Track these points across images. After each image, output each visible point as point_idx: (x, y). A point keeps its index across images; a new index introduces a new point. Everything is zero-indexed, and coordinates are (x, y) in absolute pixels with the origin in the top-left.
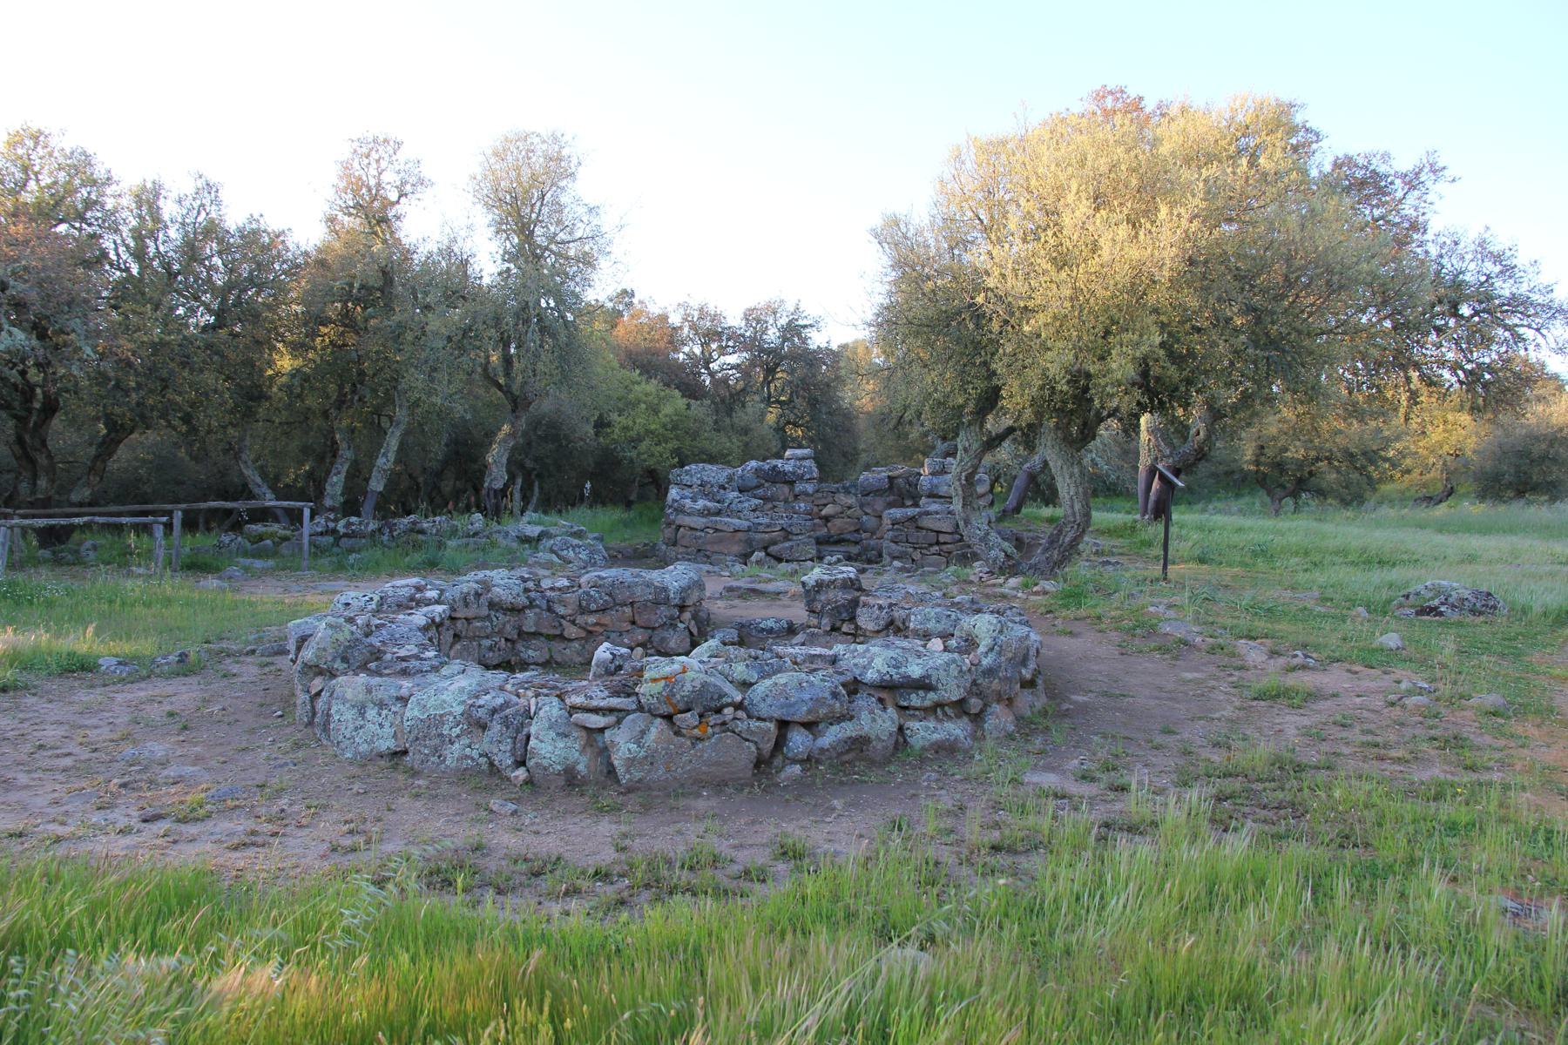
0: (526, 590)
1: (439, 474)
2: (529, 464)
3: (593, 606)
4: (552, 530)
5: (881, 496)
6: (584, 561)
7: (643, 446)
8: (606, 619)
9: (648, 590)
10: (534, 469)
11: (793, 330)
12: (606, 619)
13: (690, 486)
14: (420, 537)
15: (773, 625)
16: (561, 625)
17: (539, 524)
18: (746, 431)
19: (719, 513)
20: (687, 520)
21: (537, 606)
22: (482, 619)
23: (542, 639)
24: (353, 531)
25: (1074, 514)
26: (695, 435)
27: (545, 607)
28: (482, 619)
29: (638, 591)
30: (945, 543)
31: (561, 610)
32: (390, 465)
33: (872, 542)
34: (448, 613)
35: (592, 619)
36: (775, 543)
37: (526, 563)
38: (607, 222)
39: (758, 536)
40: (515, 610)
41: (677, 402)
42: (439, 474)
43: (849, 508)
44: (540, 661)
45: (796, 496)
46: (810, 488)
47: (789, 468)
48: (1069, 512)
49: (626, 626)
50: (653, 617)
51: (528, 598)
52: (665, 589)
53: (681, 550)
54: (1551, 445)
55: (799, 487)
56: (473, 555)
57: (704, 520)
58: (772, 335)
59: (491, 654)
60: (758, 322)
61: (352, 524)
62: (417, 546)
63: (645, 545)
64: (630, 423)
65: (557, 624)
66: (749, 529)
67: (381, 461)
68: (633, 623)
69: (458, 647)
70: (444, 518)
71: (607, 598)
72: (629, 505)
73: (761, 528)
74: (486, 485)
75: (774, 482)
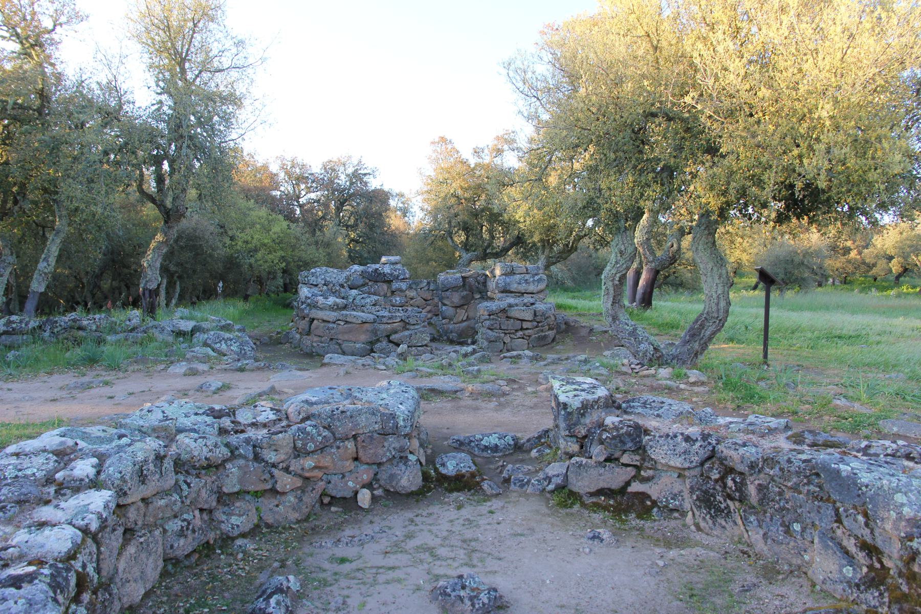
0: (222, 431)
1: (99, 276)
2: (172, 268)
3: (311, 446)
4: (205, 325)
5: (457, 291)
6: (236, 353)
7: (259, 255)
8: (326, 461)
9: (374, 419)
10: (176, 272)
11: (356, 177)
12: (326, 461)
13: (316, 286)
14: (81, 333)
15: (496, 441)
16: (272, 476)
17: (191, 318)
18: (328, 245)
19: (345, 307)
20: (321, 314)
21: (240, 456)
22: (166, 493)
23: (248, 497)
24: (14, 329)
25: (718, 310)
26: (294, 248)
27: (251, 456)
28: (166, 493)
29: (362, 420)
30: (527, 329)
31: (271, 457)
32: (51, 269)
33: (451, 327)
34: (113, 505)
35: (309, 463)
36: (396, 332)
37: (183, 357)
38: (252, 53)
39: (382, 327)
40: (213, 467)
41: (280, 225)
42: (99, 276)
43: (412, 299)
44: (247, 529)
45: (393, 292)
46: (404, 286)
47: (387, 270)
48: (714, 309)
49: (349, 465)
50: (381, 451)
51: (227, 445)
52: (393, 416)
53: (316, 339)
54: (804, 256)
55: (395, 285)
56: (134, 349)
57: (335, 314)
58: (343, 180)
59: (182, 541)
60: (333, 170)
61: (13, 322)
62: (78, 342)
63: (278, 333)
64: (249, 238)
65: (267, 476)
66: (375, 321)
67: (42, 265)
68: (356, 459)
69: (131, 549)
70: (103, 315)
71: (326, 433)
72: (246, 298)
73: (384, 320)
74: (142, 285)
75: (376, 282)
